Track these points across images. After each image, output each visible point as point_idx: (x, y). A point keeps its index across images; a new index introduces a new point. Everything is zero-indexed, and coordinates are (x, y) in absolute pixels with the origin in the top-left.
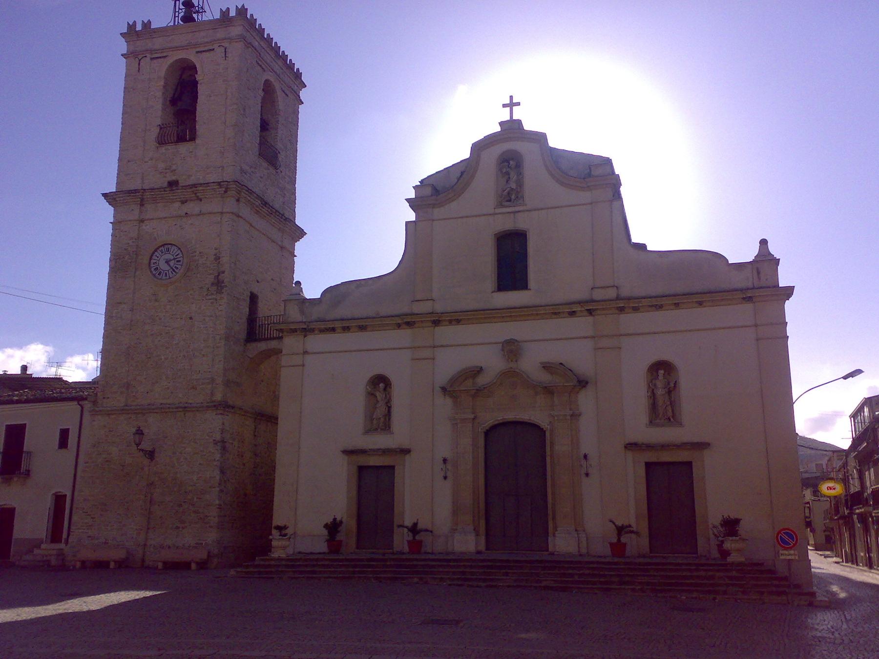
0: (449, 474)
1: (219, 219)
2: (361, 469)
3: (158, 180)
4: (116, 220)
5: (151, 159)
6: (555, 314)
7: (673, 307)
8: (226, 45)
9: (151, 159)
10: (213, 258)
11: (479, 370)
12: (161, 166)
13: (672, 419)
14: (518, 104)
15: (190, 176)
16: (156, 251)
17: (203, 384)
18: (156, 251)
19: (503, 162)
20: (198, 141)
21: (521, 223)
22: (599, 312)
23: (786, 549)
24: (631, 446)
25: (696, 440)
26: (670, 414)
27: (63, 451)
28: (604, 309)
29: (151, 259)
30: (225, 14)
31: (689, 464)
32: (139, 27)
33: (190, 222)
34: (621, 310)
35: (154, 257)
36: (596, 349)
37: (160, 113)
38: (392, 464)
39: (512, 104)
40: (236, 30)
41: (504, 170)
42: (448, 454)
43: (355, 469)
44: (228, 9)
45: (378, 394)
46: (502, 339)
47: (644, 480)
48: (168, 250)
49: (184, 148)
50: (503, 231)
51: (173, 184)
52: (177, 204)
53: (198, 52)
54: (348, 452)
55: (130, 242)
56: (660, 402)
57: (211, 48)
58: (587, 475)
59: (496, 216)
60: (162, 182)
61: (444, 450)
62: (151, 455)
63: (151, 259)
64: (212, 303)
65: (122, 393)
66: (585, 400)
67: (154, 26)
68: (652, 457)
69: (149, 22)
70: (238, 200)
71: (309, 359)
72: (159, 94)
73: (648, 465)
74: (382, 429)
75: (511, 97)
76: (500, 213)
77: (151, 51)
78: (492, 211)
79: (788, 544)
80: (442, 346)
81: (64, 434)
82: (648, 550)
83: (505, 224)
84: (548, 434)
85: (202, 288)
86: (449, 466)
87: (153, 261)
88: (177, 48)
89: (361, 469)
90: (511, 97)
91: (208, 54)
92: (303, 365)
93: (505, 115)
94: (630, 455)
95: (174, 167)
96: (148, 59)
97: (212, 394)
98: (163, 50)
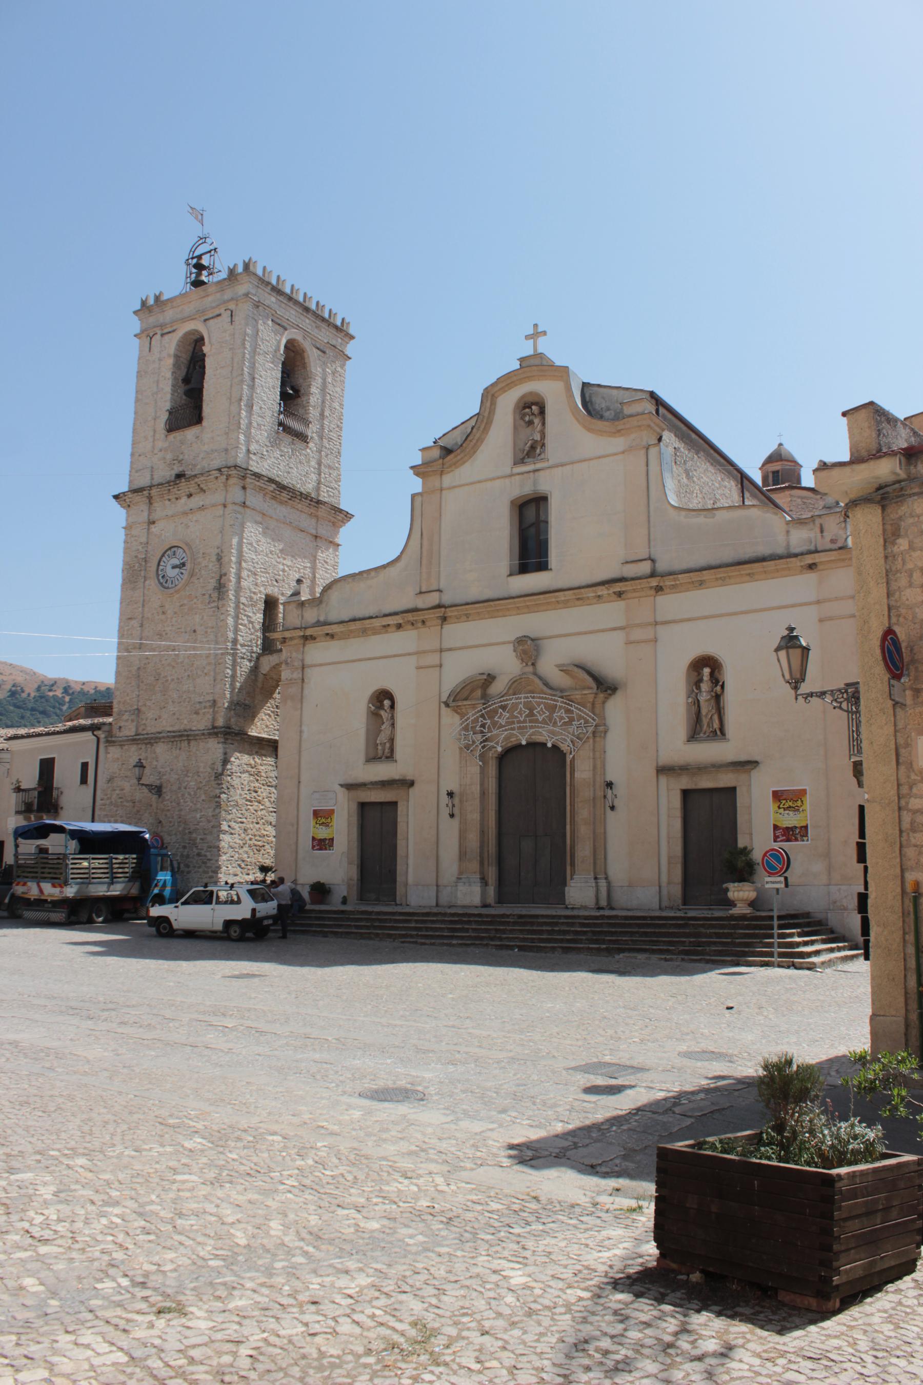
0: (456, 811)
1: (221, 512)
2: (363, 806)
3: (165, 473)
4: (685, 1316)
5: (161, 450)
6: (578, 599)
7: (748, 578)
8: (232, 306)
9: (161, 450)
10: (214, 558)
11: (490, 678)
12: (169, 456)
13: (718, 733)
14: (544, 333)
15: (195, 465)
16: (163, 556)
17: (205, 707)
18: (163, 556)
19: (524, 408)
20: (205, 423)
21: (544, 487)
22: (630, 595)
23: (770, 874)
24: (663, 770)
25: (743, 758)
26: (716, 725)
27: (84, 786)
28: (634, 591)
29: (159, 565)
30: (232, 272)
31: (733, 790)
32: (151, 301)
33: (195, 519)
34: (659, 589)
35: (162, 563)
36: (629, 643)
37: (169, 396)
38: (394, 799)
39: (536, 334)
40: (243, 288)
41: (527, 418)
42: (453, 786)
43: (354, 807)
44: (235, 265)
45: (382, 713)
46: (513, 638)
47: (678, 813)
48: (174, 553)
49: (190, 433)
50: (511, 510)
51: (179, 476)
52: (184, 500)
53: (205, 320)
54: (350, 787)
55: (140, 548)
56: (704, 711)
57: (217, 312)
58: (612, 808)
59: (513, 478)
60: (169, 474)
61: (450, 782)
62: (158, 790)
63: (159, 565)
64: (214, 612)
65: (133, 721)
66: (614, 708)
67: (165, 297)
68: (686, 783)
69: (161, 293)
70: (244, 488)
71: (662, 631)
72: (169, 375)
73: (686, 793)
74: (387, 757)
75: (536, 326)
76: (519, 474)
77: (162, 326)
78: (508, 471)
79: (775, 869)
80: (409, 654)
81: (85, 766)
82: (680, 901)
83: (522, 488)
84: (569, 758)
85: (204, 595)
86: (456, 800)
87: (161, 568)
88: (184, 320)
89: (363, 806)
90: (536, 326)
91: (215, 320)
92: (441, 666)
93: (527, 349)
94: (663, 780)
95: (181, 457)
96: (158, 337)
97: (214, 719)
98: (173, 322)
